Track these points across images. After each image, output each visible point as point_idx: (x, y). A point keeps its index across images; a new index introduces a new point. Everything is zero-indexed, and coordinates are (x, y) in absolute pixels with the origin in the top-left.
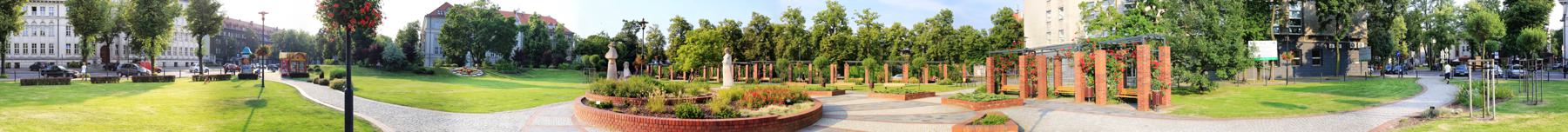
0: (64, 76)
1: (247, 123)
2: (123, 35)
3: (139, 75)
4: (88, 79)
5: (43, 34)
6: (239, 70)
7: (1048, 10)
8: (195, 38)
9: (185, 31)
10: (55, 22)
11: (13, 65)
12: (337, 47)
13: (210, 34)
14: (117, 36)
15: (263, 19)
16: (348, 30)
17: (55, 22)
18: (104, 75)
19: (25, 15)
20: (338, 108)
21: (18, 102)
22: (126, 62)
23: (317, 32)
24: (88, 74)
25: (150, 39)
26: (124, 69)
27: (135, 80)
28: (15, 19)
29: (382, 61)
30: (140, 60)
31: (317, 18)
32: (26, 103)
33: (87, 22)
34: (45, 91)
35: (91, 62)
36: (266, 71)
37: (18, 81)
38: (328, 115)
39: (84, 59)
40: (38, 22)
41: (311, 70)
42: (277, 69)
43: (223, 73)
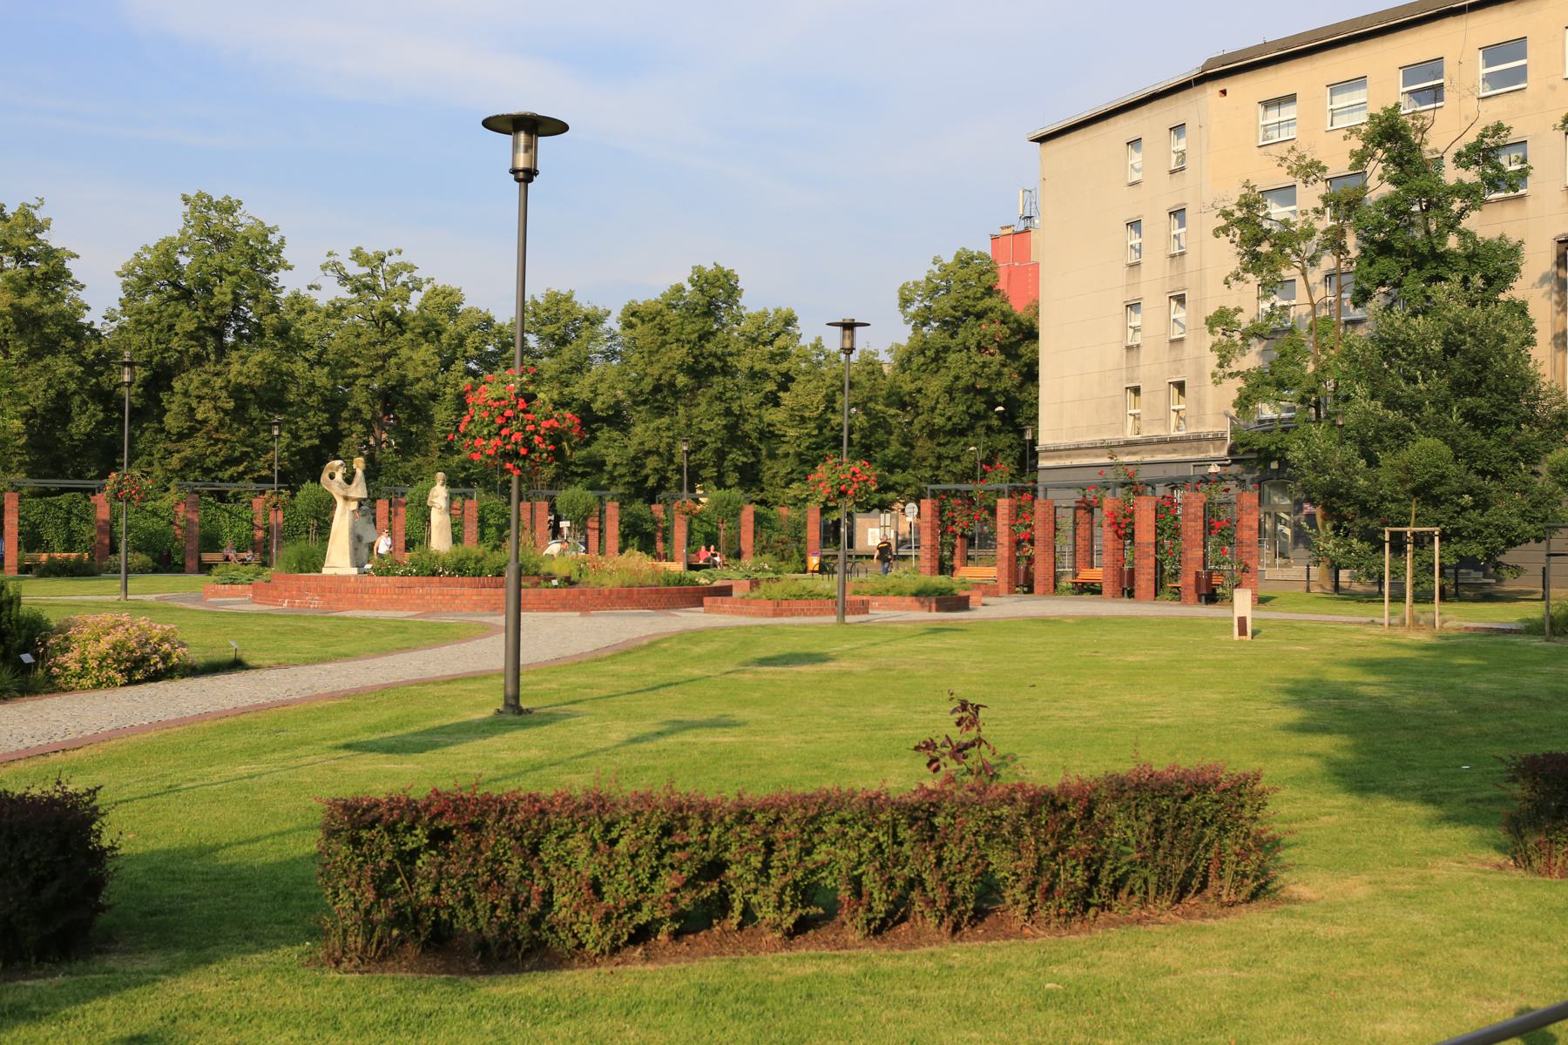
7: (1129, 298)
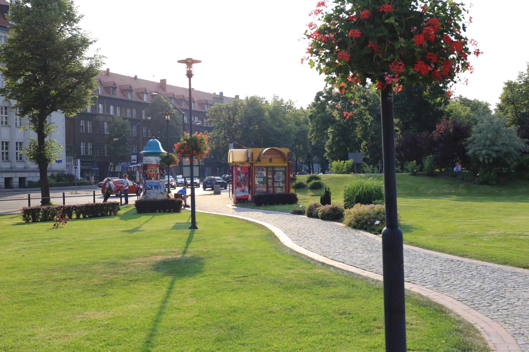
1: (160, 313)
6: (137, 191)
8: (27, 118)
12: (358, 132)
13: (65, 109)
15: (190, 75)
16: (386, 89)
20: (366, 274)
23: (311, 100)
29: (466, 161)
31: (312, 64)
36: (199, 191)
38: (343, 290)
41: (300, 187)
42: (224, 186)
43: (100, 200)
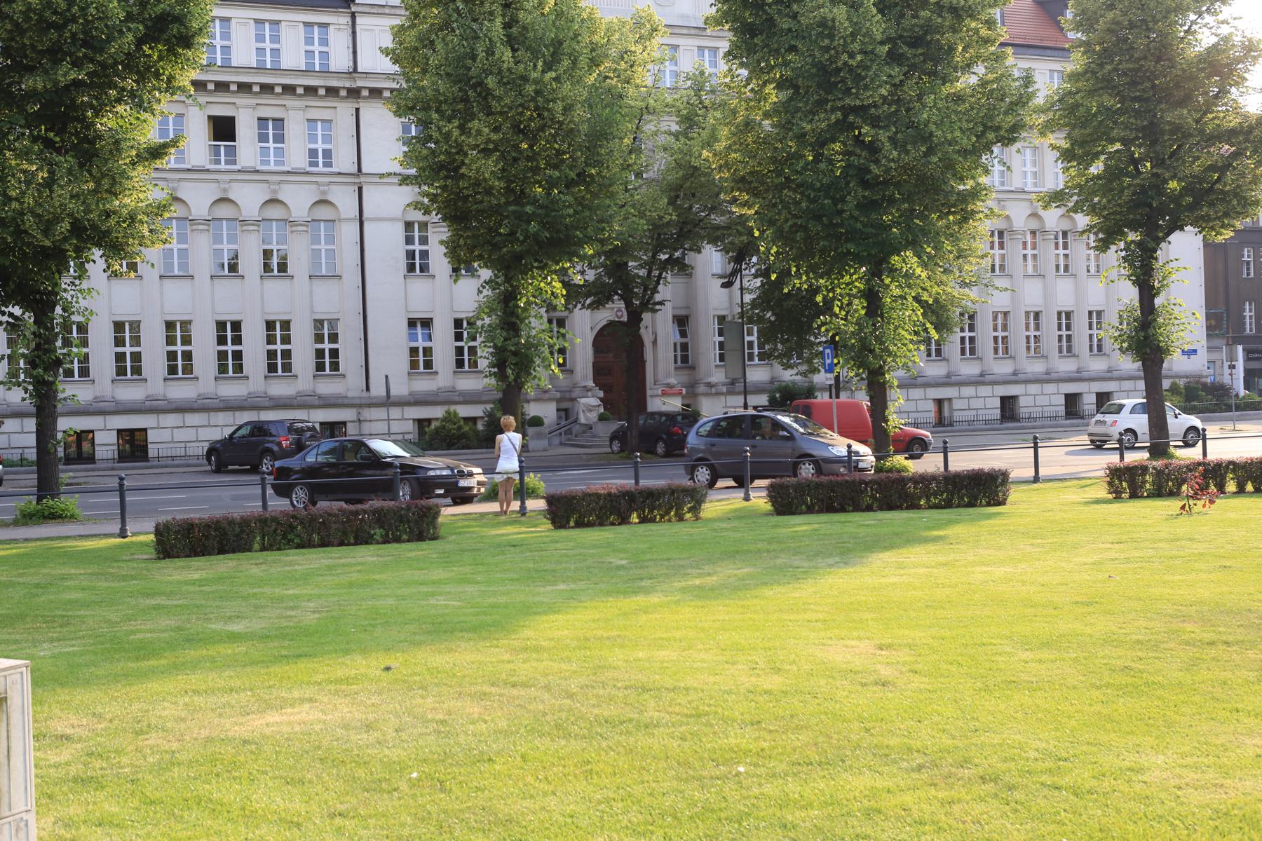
0: (404, 493)
2: (711, 260)
3: (807, 471)
4: (536, 505)
5: (275, 266)
8: (1114, 255)
9: (1053, 218)
10: (344, 200)
11: (106, 442)
13: (1202, 223)
14: (682, 268)
17: (344, 200)
18: (617, 481)
19: (170, 161)
21: (145, 650)
22: (733, 406)
24: (532, 479)
25: (856, 278)
26: (724, 443)
27: (784, 503)
28: (113, 184)
30: (810, 392)
32: (192, 654)
33: (521, 197)
34: (306, 578)
35: (547, 411)
37: (143, 534)
39: (510, 400)
40: (249, 198)
